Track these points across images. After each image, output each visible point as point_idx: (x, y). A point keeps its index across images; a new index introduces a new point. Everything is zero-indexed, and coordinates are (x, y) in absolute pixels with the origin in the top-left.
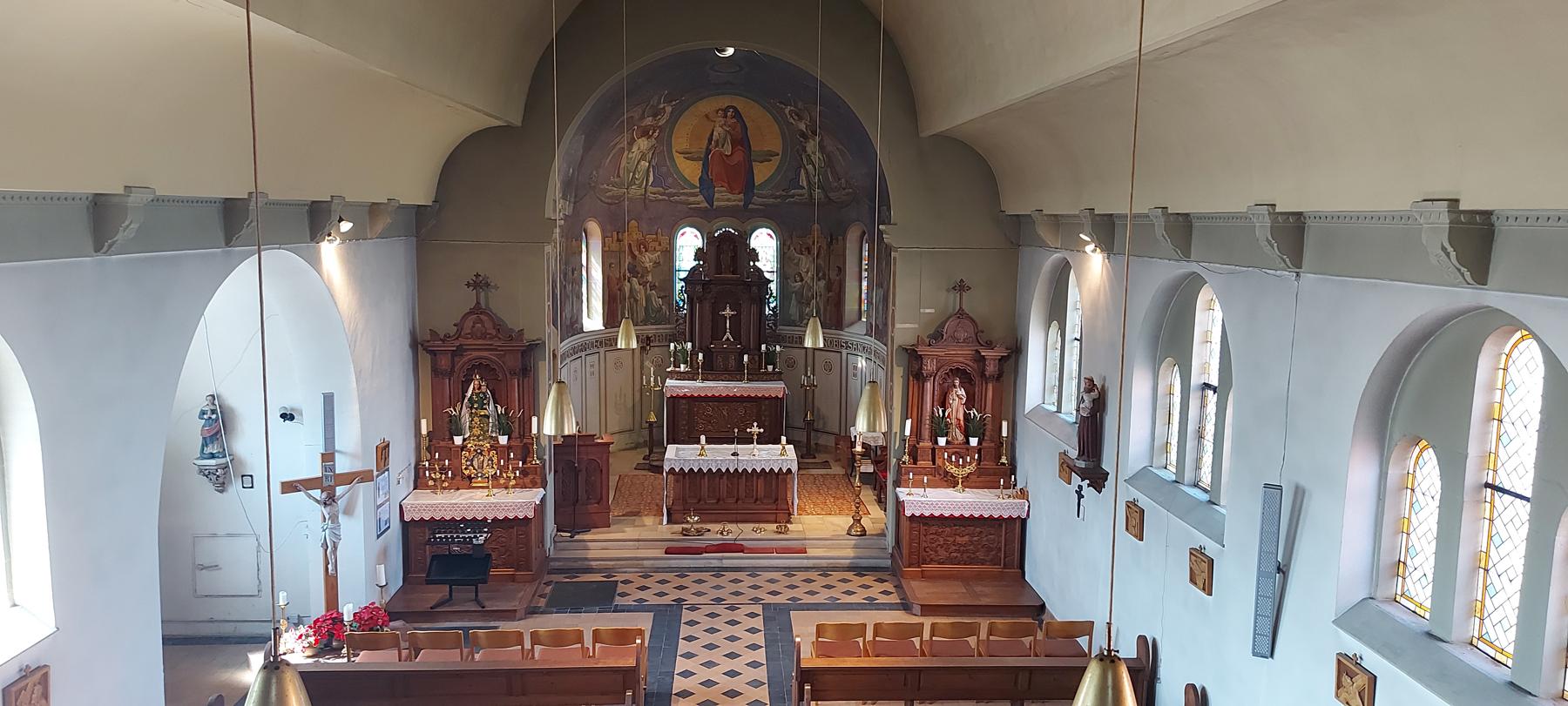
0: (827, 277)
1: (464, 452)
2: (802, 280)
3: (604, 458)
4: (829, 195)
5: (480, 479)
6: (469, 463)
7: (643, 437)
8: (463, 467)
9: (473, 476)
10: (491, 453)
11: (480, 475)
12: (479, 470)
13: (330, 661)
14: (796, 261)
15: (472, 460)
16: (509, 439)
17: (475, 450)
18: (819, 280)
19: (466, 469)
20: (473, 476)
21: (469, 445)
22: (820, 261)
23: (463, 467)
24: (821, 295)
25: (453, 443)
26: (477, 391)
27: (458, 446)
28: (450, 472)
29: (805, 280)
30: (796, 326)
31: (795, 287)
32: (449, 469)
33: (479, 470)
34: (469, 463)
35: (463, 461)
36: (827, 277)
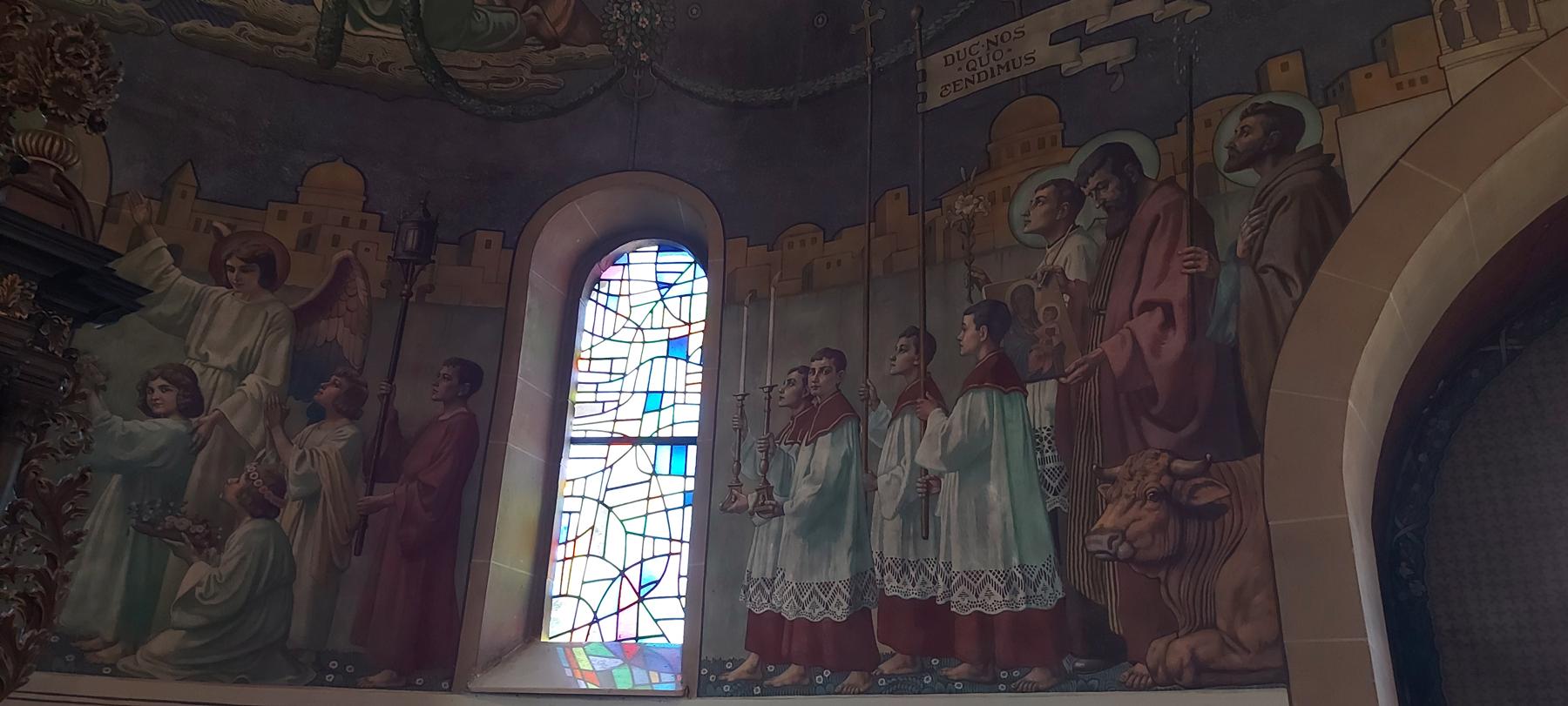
0: (372, 409)
2: (192, 404)
4: (444, 57)
14: (168, 309)
18: (317, 415)
22: (334, 330)
24: (310, 500)
29: (221, 405)
30: (96, 670)
31: (130, 439)
36: (372, 409)
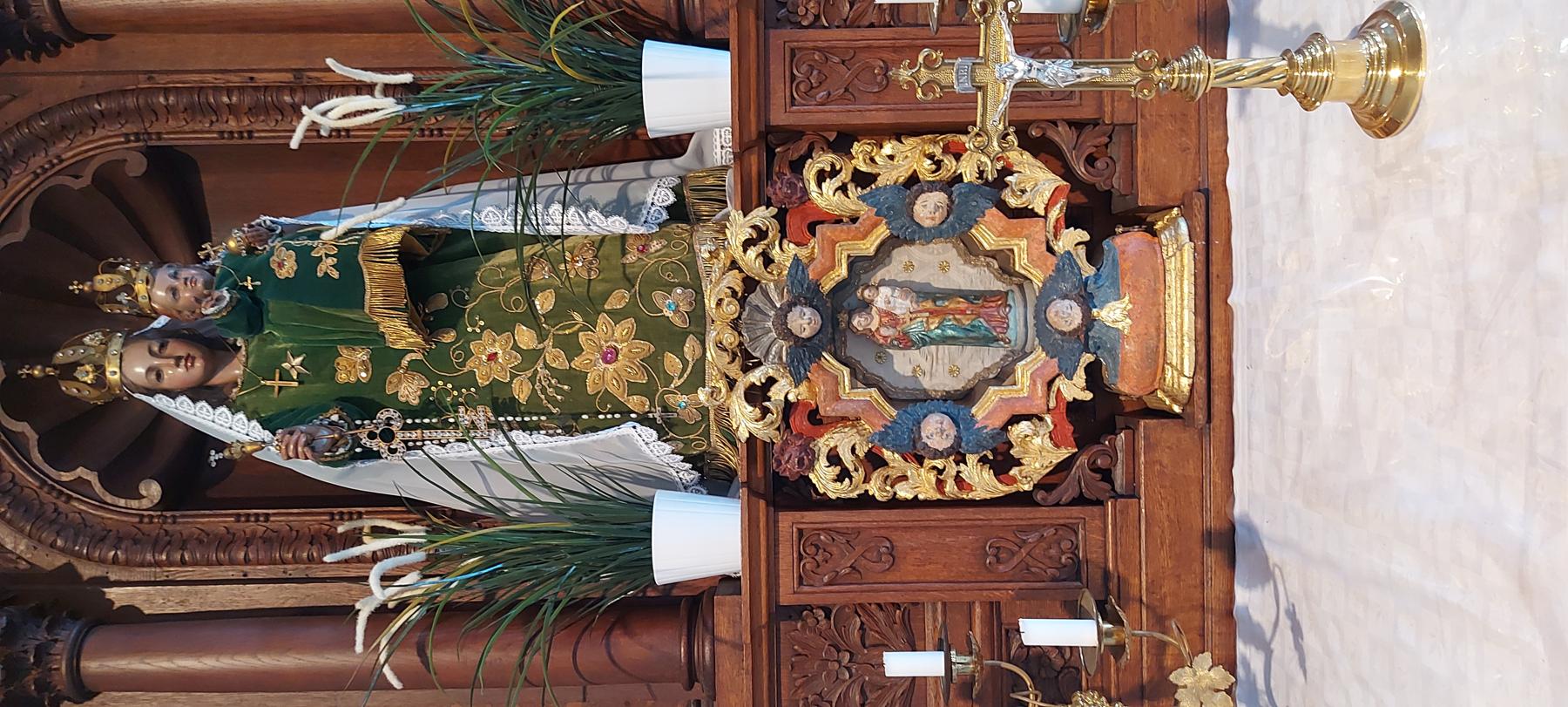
1: (823, 477)
3: (945, 226)
5: (1113, 314)
6: (936, 431)
7: (879, 75)
8: (983, 483)
9: (1074, 388)
10: (825, 197)
11: (1066, 314)
12: (1017, 319)
13: (580, 440)
15: (912, 401)
16: (686, 34)
17: (803, 355)
19: (1002, 461)
20: (1074, 388)
21: (744, 420)
23: (983, 483)
25: (728, 582)
26: (234, 370)
27: (758, 541)
28: (1039, 632)
32: (1003, 634)
33: (1017, 319)
34: (936, 431)
35: (919, 484)
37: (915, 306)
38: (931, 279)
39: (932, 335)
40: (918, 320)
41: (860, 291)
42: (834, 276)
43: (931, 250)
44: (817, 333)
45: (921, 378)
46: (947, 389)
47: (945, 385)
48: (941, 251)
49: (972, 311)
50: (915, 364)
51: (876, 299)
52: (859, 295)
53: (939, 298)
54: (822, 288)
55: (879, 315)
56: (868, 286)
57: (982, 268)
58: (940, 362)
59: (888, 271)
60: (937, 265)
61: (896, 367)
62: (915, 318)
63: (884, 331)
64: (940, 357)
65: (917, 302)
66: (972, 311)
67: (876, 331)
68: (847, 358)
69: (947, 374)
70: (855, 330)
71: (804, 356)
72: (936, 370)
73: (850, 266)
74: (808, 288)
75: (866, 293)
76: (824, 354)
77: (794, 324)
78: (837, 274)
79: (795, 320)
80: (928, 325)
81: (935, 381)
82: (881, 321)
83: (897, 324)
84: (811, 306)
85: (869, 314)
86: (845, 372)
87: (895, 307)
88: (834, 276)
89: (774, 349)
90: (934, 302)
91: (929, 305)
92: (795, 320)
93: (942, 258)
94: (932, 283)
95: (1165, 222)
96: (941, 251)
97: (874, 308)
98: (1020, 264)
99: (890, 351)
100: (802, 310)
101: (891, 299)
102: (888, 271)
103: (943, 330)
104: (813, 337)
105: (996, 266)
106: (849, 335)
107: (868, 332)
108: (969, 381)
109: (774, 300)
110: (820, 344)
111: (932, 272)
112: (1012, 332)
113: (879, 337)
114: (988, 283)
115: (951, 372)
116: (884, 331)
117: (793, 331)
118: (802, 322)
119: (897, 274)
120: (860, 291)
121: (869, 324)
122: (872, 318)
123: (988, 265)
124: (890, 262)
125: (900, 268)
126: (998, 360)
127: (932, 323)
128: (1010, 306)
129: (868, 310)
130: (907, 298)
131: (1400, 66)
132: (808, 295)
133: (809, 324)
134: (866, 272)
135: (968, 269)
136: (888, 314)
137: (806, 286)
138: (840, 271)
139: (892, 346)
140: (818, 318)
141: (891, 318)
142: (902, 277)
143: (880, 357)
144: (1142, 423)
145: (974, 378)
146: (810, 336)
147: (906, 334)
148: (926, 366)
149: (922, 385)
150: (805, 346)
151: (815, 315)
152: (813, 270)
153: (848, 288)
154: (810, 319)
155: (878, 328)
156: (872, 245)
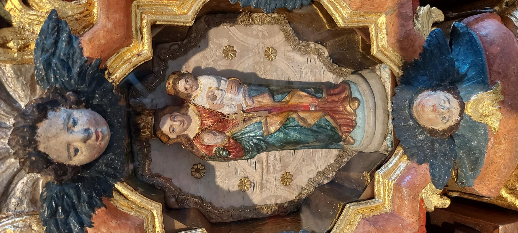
37: (250, 103)
38: (257, 68)
39: (271, 140)
40: (255, 121)
41: (171, 81)
42: (129, 55)
43: (255, 32)
44: (105, 153)
45: (249, 192)
46: (279, 202)
47: (277, 197)
48: (266, 33)
49: (316, 106)
50: (241, 175)
51: (194, 94)
52: (169, 87)
53: (278, 92)
54: (110, 74)
55: (200, 116)
56: (181, 76)
57: (312, 56)
58: (271, 169)
59: (205, 57)
60: (262, 51)
61: (219, 182)
62: (250, 119)
63: (208, 139)
64: (271, 163)
65: (251, 97)
66: (316, 106)
67: (195, 138)
68: (152, 176)
69: (278, 184)
70: (164, 139)
71: (79, 197)
72: (267, 181)
73: (156, 43)
74: (82, 74)
75: (182, 85)
76: (118, 186)
77: (53, 142)
78: (135, 52)
79: (55, 136)
80: (267, 127)
81: (266, 193)
82: (202, 123)
83: (225, 127)
84: (89, 106)
85: (186, 115)
86: (155, 212)
87: (222, 105)
88: (129, 55)
89: (20, 185)
90: (272, 94)
91: (266, 100)
92: (55, 136)
93: (268, 43)
94: (258, 73)
95: (504, 6)
96: (266, 33)
97: (191, 106)
98: (378, 47)
99: (212, 163)
100: (69, 117)
101: (218, 93)
102: (205, 57)
103: (286, 134)
104: (96, 160)
105: (326, 54)
106: (154, 143)
107: (184, 141)
108: (302, 188)
109: (15, 96)
110: (111, 171)
111: (257, 58)
112: (360, 131)
113: (199, 147)
114: (318, 73)
115: (283, 179)
116: (208, 139)
117: (53, 156)
118: (70, 137)
119: (215, 61)
120: (171, 81)
121: (185, 130)
122: (190, 121)
123: (319, 54)
124: (207, 46)
125: (219, 54)
126: (332, 162)
127: (271, 125)
128: (356, 99)
129: (183, 111)
130: (238, 92)
131: (37, 130)
132: (83, 88)
133: (85, 141)
134: (174, 58)
135: (298, 57)
136: (212, 113)
137: (76, 70)
138: (140, 48)
139: (219, 157)
140: (104, 129)
141: (15, 20)
142: (222, 65)
143: (197, 171)
144: (500, 227)
145: (309, 185)
146: (88, 161)
147: (237, 140)
148: (255, 176)
149: (251, 201)
150: (81, 179)
151: (97, 124)
152: (90, 40)
153: (150, 78)
154: (86, 130)
155: (198, 135)
156: (189, 11)
